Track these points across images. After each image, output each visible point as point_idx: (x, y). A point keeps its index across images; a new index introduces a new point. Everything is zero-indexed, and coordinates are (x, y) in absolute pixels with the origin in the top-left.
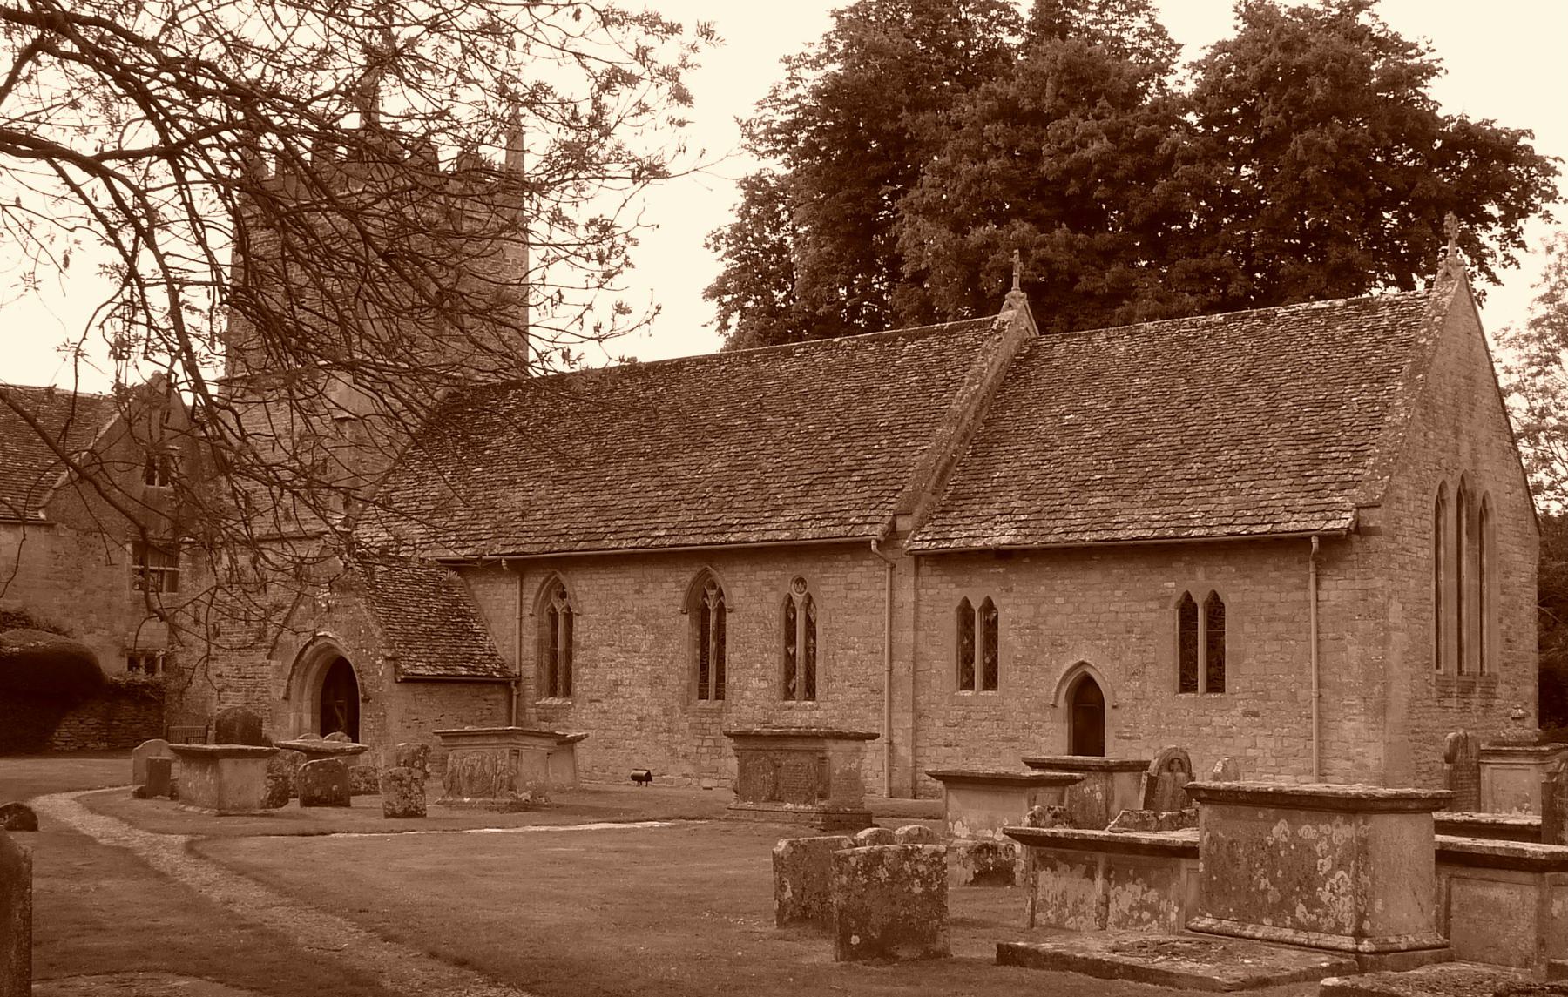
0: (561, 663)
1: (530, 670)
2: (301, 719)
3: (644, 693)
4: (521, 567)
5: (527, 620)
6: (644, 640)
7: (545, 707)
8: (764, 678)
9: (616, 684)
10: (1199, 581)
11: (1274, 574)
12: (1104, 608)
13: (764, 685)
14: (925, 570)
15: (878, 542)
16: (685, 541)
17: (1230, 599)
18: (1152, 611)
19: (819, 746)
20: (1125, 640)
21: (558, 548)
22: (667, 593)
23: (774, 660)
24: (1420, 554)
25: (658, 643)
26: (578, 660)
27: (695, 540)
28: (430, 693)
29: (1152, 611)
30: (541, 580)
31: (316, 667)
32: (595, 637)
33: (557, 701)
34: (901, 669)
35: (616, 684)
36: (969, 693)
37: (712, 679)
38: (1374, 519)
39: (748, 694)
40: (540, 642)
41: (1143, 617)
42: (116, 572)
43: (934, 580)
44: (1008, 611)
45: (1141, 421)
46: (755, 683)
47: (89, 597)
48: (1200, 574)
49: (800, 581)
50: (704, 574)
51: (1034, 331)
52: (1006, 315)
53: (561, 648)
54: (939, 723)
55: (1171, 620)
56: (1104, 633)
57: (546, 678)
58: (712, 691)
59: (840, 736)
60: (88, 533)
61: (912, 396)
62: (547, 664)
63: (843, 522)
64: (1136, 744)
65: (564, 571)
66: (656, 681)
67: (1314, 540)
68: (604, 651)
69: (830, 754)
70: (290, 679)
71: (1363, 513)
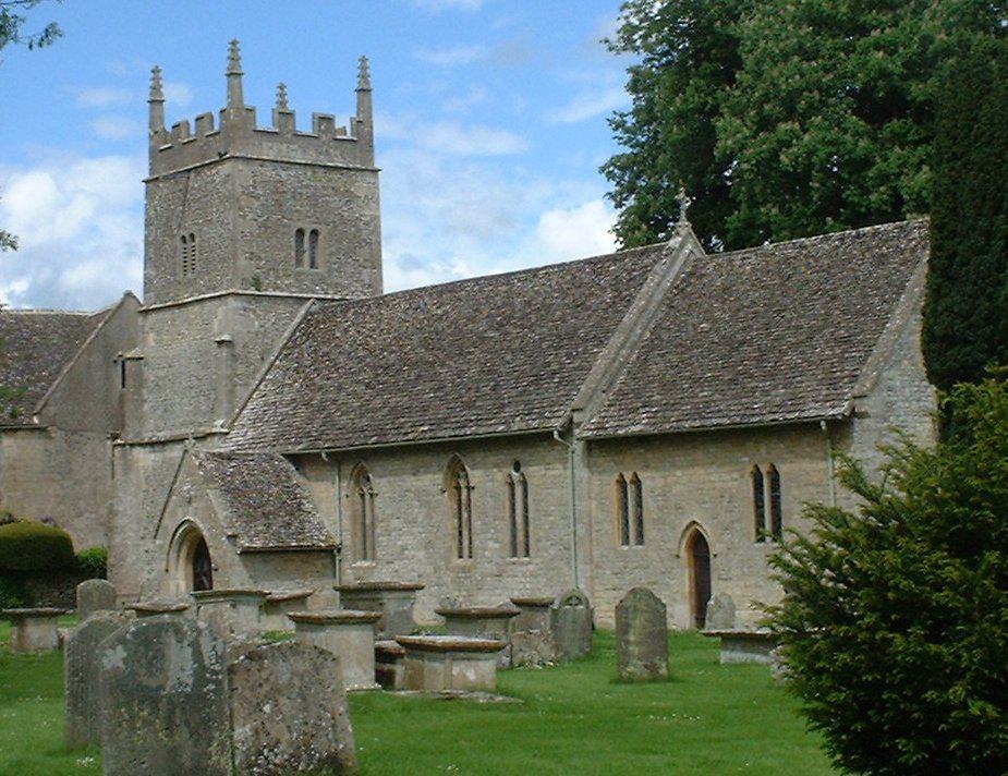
0: (369, 533)
1: (347, 540)
2: (178, 586)
3: (421, 554)
4: (339, 459)
5: (344, 500)
6: (419, 513)
7: (361, 568)
8: (496, 541)
9: (404, 548)
10: (762, 455)
11: (808, 449)
12: (707, 479)
13: (497, 546)
14: (596, 452)
15: (559, 432)
16: (439, 435)
17: (782, 469)
18: (736, 480)
19: (379, 596)
20: (720, 502)
21: (358, 442)
22: (431, 480)
23: (504, 526)
24: (921, 429)
25: (429, 516)
26: (378, 531)
27: (446, 434)
28: (265, 561)
29: (736, 480)
30: (352, 467)
31: (684, 542)
32: (389, 511)
33: (366, 564)
34: (581, 531)
35: (404, 548)
36: (626, 548)
37: (466, 543)
38: (862, 407)
39: (486, 553)
40: (354, 518)
41: (730, 485)
42: (99, 465)
43: (601, 460)
44: (648, 483)
45: (744, 329)
46: (491, 544)
47: (77, 487)
48: (763, 450)
49: (517, 467)
50: (455, 458)
51: (700, 253)
52: (674, 242)
53: (368, 522)
54: (608, 572)
55: (613, 492)
56: (707, 499)
57: (359, 547)
58: (466, 552)
59: (392, 589)
60: (74, 432)
61: (605, 310)
62: (360, 534)
63: (541, 416)
64: (730, 584)
65: (366, 459)
66: (429, 545)
67: (823, 423)
68: (395, 523)
69: (385, 601)
70: (168, 553)
71: (857, 402)
